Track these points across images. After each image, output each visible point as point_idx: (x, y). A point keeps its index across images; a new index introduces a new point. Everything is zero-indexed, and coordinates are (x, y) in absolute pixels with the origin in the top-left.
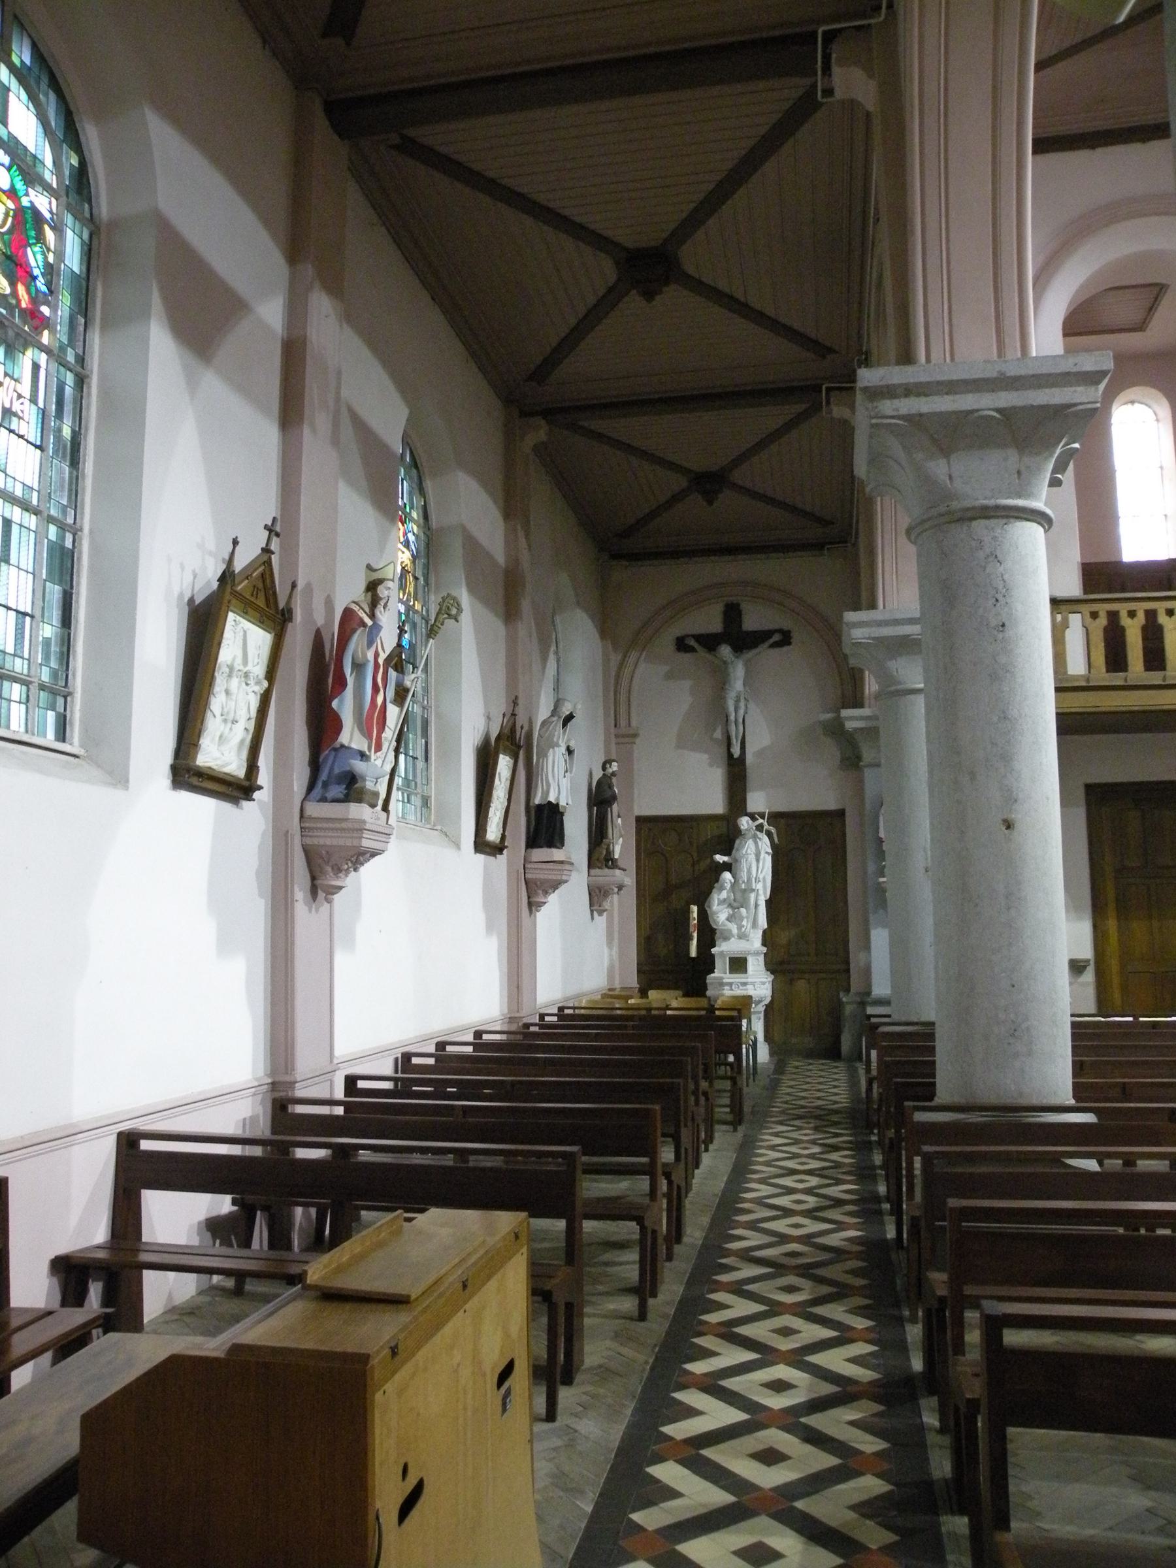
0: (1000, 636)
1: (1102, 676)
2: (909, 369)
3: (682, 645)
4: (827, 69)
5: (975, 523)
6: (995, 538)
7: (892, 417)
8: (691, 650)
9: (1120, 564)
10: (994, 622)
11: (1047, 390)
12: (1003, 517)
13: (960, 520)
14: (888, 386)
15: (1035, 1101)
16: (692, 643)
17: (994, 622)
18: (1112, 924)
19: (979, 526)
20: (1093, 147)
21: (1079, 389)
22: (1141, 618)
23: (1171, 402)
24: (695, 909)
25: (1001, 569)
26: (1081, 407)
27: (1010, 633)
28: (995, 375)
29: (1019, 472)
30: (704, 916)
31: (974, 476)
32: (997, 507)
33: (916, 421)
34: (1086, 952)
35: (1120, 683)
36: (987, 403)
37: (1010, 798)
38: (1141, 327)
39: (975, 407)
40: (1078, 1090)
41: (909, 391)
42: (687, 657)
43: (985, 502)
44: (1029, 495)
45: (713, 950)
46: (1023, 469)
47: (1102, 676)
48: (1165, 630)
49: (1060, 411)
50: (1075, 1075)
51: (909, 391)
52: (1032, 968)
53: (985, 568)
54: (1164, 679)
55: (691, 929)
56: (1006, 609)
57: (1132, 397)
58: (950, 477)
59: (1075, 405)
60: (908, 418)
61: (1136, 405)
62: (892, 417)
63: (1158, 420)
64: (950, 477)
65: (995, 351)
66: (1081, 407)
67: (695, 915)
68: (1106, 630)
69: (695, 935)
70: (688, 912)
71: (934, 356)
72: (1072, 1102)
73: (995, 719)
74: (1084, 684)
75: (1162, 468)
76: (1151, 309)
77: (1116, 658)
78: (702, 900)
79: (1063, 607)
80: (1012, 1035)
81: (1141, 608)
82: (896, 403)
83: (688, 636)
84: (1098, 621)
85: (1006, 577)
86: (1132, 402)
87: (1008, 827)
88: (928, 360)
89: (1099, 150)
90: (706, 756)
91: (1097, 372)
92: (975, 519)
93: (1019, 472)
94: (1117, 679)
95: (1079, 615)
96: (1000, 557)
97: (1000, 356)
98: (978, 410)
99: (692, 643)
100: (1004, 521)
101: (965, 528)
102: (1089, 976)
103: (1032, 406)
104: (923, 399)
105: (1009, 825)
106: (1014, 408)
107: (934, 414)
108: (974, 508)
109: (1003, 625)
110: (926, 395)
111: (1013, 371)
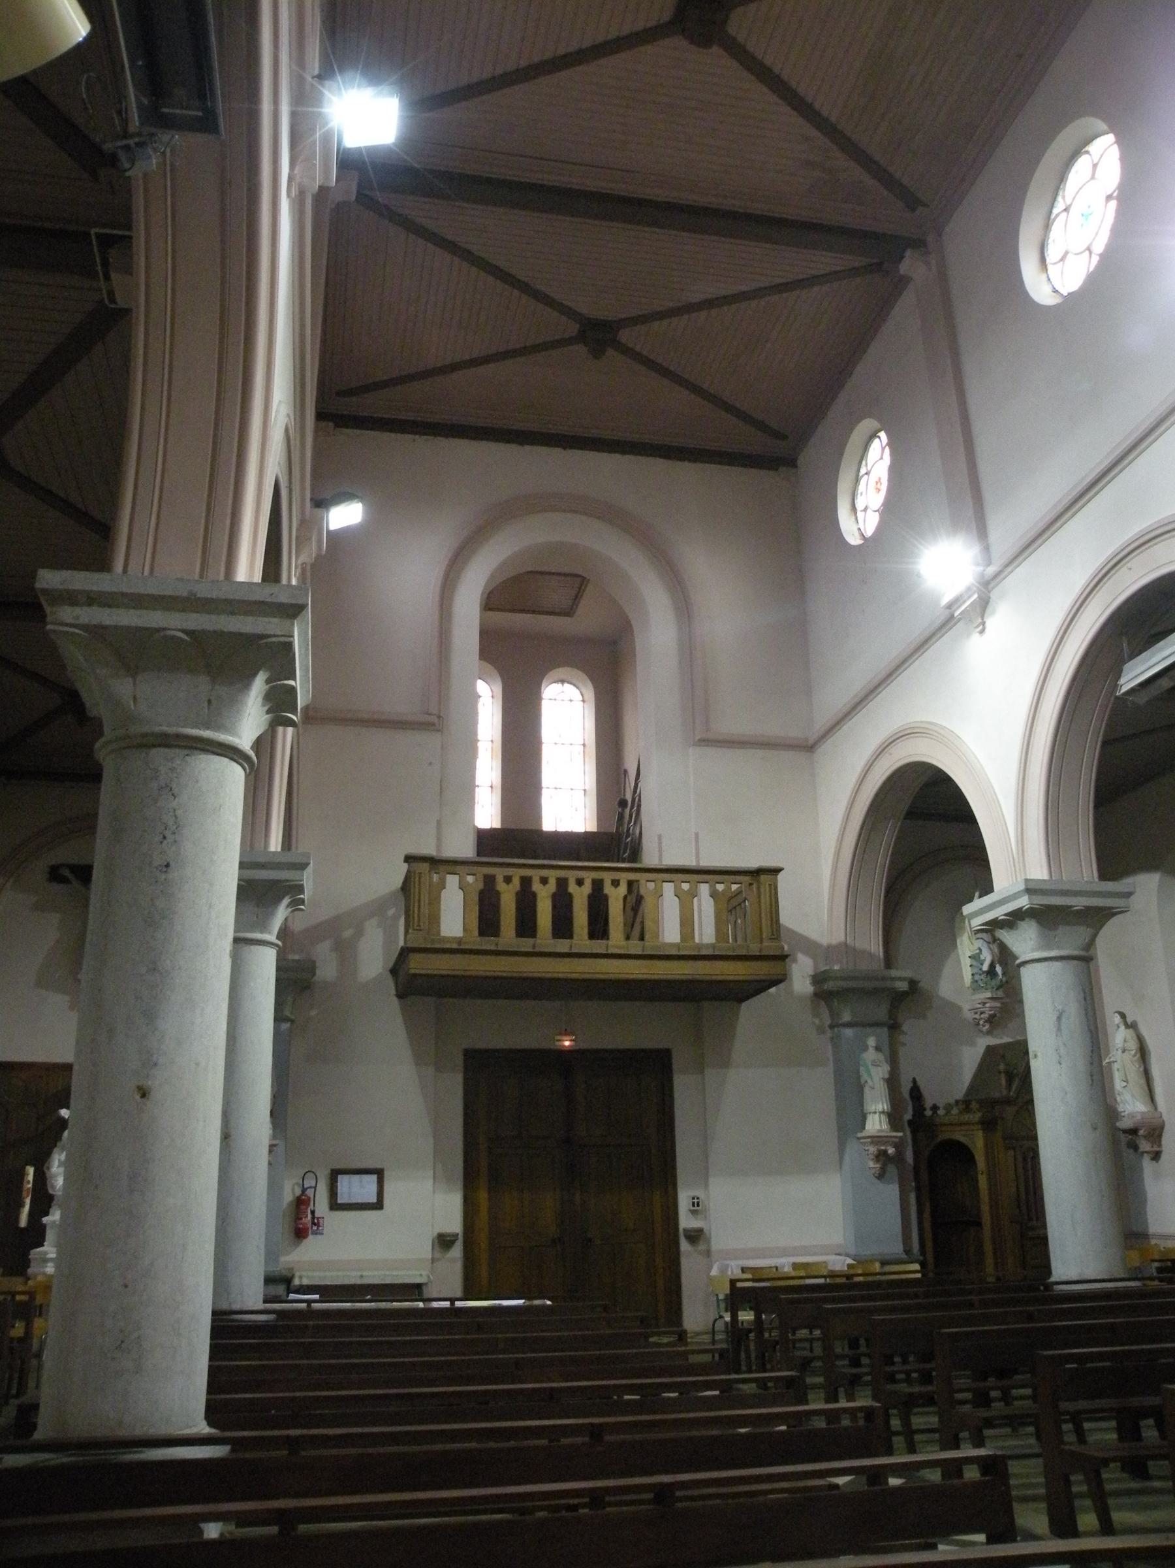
0: (163, 877)
1: (476, 941)
2: (104, 576)
3: (55, 875)
4: (107, 277)
5: (154, 751)
6: (172, 770)
7: (71, 625)
8: (63, 880)
9: (540, 833)
10: (158, 861)
11: (241, 618)
12: (186, 747)
13: (141, 746)
14: (67, 591)
15: (139, 1432)
16: (66, 873)
17: (158, 861)
18: (483, 1196)
19: (158, 754)
20: (521, 444)
21: (275, 620)
22: (552, 886)
23: (595, 688)
24: (31, 1170)
25: (174, 804)
26: (274, 639)
27: (174, 875)
28: (185, 594)
29: (209, 701)
30: (41, 1179)
31: (156, 700)
32: (178, 736)
33: (98, 632)
34: (454, 1224)
35: (493, 948)
36: (175, 622)
37: (149, 1062)
38: (569, 613)
39: (166, 625)
40: (212, 1412)
41: (92, 599)
42: (56, 887)
43: (165, 729)
44: (218, 728)
45: (45, 1220)
46: (212, 698)
47: (476, 941)
48: (539, 899)
49: (253, 640)
50: (209, 1392)
51: (92, 599)
52: (152, 1264)
53: (156, 801)
54: (534, 946)
55: (24, 1194)
56: (174, 848)
57: (563, 677)
58: (135, 698)
59: (269, 636)
60: (85, 627)
61: (566, 685)
62: (71, 625)
63: (583, 701)
64: (135, 698)
65: (198, 570)
66: (274, 639)
67: (30, 1177)
68: (590, 897)
69: (28, 1201)
70: (22, 1174)
71: (133, 568)
72: (204, 1429)
73: (143, 970)
74: (455, 946)
75: (584, 745)
76: (576, 597)
77: (488, 922)
78: (41, 1163)
79: (442, 868)
80: (119, 1347)
81: (588, 877)
82: (78, 611)
83: (62, 865)
84: (511, 886)
85: (179, 813)
86: (563, 682)
87: (144, 1095)
88: (125, 571)
89: (527, 448)
90: (67, 998)
91: (292, 605)
92: (154, 746)
93: (209, 701)
94: (488, 943)
95: (457, 877)
96: (176, 791)
97: (201, 577)
98: (164, 629)
99: (66, 873)
100: (186, 752)
101: (144, 755)
102: (457, 1251)
103: (223, 632)
104: (107, 611)
105: (144, 1093)
106: (204, 631)
107: (116, 627)
108: (153, 734)
109: (167, 866)
110: (110, 606)
111: (204, 591)
